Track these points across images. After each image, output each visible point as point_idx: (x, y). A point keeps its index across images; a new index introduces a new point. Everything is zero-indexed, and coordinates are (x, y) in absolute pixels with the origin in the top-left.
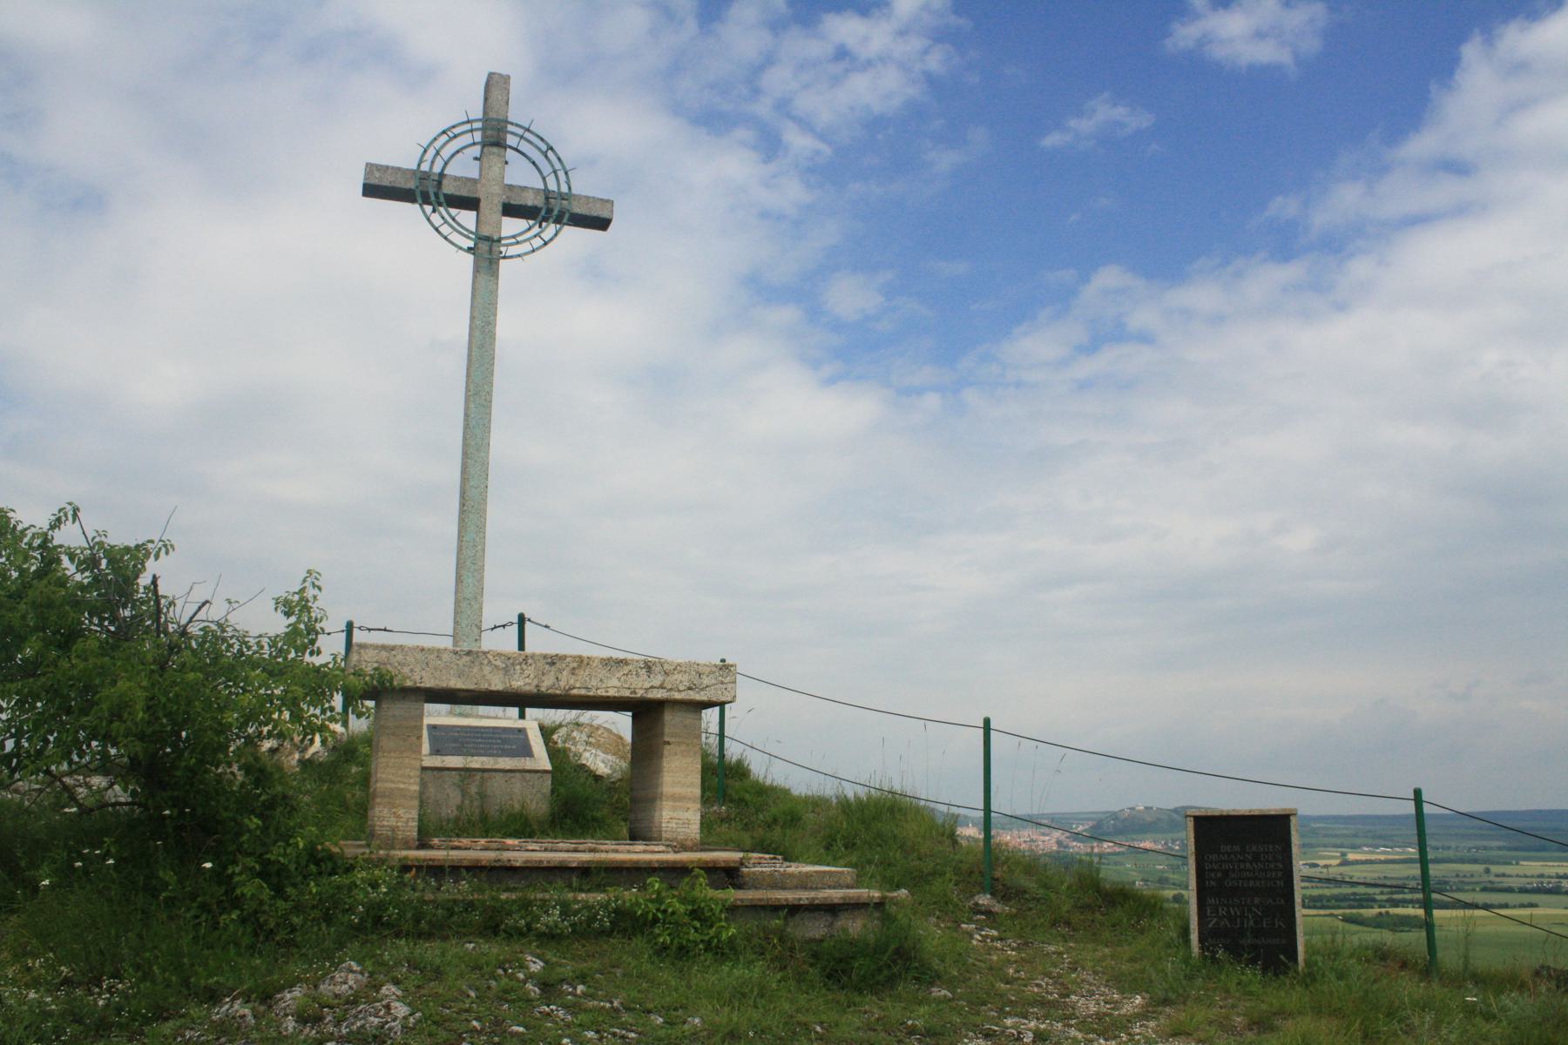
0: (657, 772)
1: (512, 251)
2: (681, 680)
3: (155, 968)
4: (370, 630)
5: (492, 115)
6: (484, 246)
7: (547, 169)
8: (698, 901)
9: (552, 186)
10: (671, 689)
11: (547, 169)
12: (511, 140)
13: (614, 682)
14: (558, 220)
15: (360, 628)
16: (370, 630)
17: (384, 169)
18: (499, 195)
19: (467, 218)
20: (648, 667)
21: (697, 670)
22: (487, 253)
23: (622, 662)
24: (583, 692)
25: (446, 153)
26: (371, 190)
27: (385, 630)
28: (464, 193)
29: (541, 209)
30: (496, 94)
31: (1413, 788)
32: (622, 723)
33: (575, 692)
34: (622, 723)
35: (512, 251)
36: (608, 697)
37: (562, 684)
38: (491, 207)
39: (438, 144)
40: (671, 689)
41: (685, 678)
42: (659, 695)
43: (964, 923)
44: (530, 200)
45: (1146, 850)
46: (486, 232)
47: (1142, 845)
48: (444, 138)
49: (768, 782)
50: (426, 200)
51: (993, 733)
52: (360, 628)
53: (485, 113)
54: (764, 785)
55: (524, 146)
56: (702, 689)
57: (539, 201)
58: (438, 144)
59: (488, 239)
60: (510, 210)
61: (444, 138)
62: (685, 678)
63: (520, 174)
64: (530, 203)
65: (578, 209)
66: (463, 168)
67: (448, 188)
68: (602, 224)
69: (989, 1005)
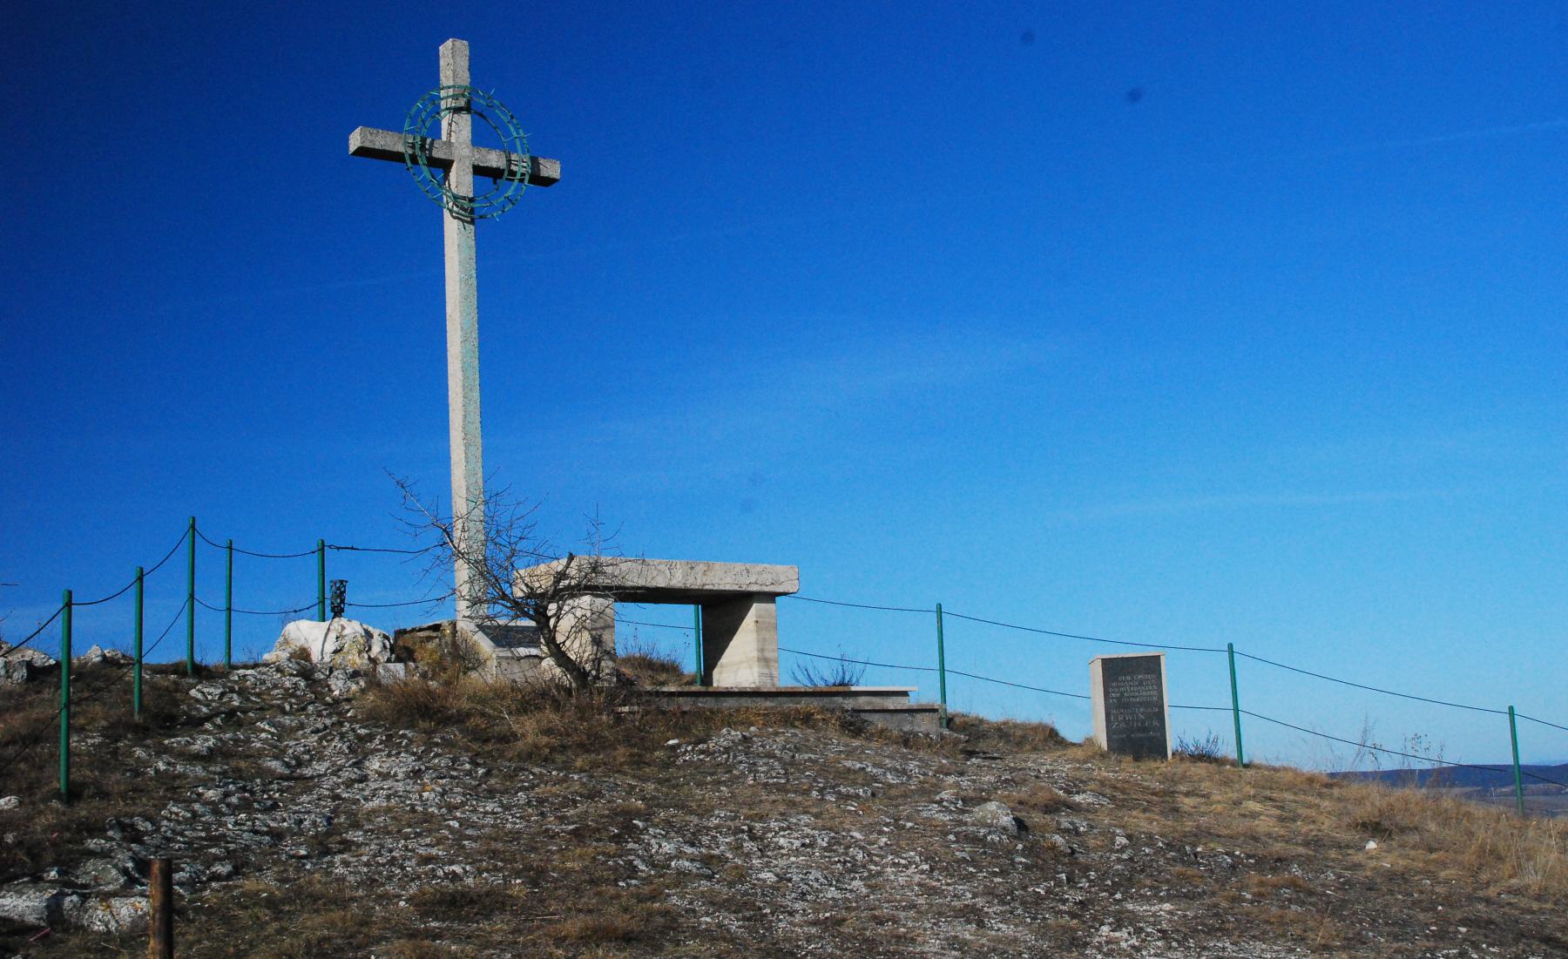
4: (338, 548)
8: (1178, 762)
10: (761, 585)
13: (729, 580)
15: (329, 547)
16: (338, 548)
18: (468, 157)
24: (710, 587)
27: (352, 548)
29: (504, 170)
32: (687, 615)
33: (707, 587)
34: (687, 615)
36: (725, 590)
37: (699, 582)
40: (761, 585)
41: (770, 577)
43: (100, 745)
45: (671, 694)
47: (665, 689)
49: (204, 663)
51: (943, 614)
52: (329, 547)
54: (201, 666)
56: (780, 584)
62: (770, 577)
64: (494, 165)
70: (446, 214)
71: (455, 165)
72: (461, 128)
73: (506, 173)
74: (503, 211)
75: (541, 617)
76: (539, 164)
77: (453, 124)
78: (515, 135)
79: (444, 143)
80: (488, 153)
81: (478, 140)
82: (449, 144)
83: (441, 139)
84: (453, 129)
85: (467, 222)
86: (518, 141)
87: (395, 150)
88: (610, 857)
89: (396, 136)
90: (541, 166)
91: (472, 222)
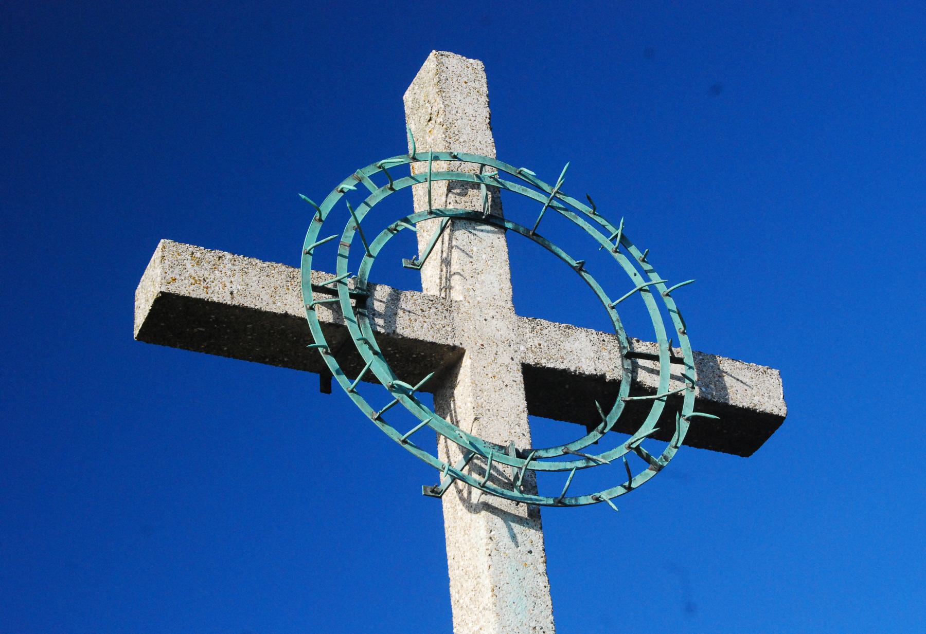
29: (616, 384)
64: (588, 368)
70: (450, 503)
71: (466, 362)
72: (479, 266)
73: (624, 392)
74: (629, 489)
75: (488, 198)
76: (720, 375)
77: (455, 254)
78: (639, 281)
79: (432, 301)
80: (568, 336)
81: (578, 469)
82: (445, 304)
83: (420, 289)
84: (455, 267)
85: (519, 520)
86: (649, 299)
87: (278, 308)
88: (147, 292)
89: (279, 272)
90: (727, 379)
91: (535, 517)
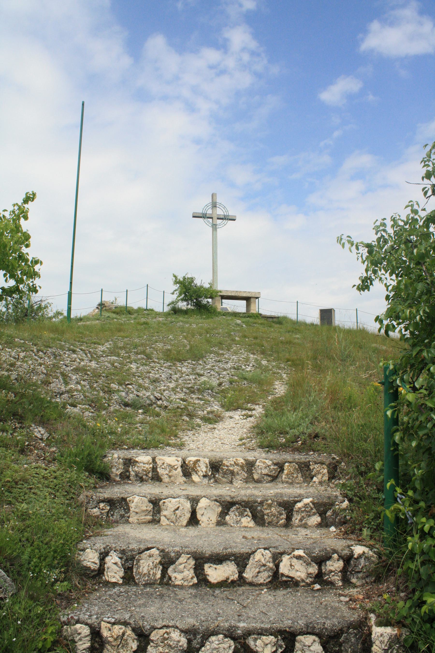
0: (250, 307)
1: (220, 227)
2: (253, 294)
3: (115, 358)
5: (214, 201)
6: (214, 226)
7: (224, 211)
9: (225, 214)
11: (224, 211)
12: (218, 206)
14: (227, 220)
17: (196, 213)
19: (210, 220)
20: (249, 292)
21: (255, 293)
22: (214, 227)
23: (246, 292)
25: (207, 209)
26: (194, 217)
28: (210, 216)
30: (214, 197)
31: (193, 276)
35: (220, 227)
38: (215, 218)
39: (205, 208)
42: (251, 296)
44: (222, 217)
46: (214, 223)
48: (225, 224)
50: (204, 218)
53: (212, 201)
55: (220, 207)
57: (223, 217)
58: (205, 208)
59: (215, 225)
60: (218, 219)
61: (225, 224)
63: (219, 212)
65: (230, 218)
66: (210, 212)
67: (207, 216)
68: (234, 220)
69: (237, 505)
